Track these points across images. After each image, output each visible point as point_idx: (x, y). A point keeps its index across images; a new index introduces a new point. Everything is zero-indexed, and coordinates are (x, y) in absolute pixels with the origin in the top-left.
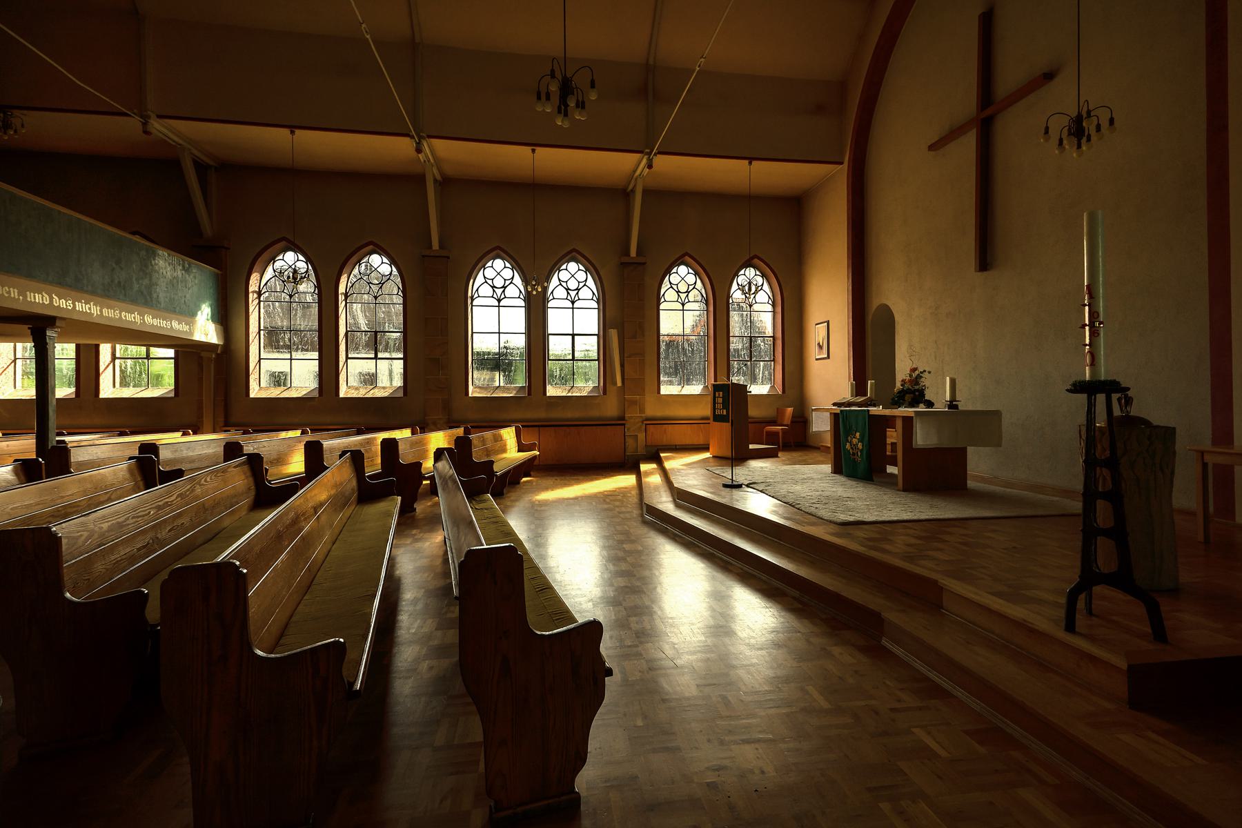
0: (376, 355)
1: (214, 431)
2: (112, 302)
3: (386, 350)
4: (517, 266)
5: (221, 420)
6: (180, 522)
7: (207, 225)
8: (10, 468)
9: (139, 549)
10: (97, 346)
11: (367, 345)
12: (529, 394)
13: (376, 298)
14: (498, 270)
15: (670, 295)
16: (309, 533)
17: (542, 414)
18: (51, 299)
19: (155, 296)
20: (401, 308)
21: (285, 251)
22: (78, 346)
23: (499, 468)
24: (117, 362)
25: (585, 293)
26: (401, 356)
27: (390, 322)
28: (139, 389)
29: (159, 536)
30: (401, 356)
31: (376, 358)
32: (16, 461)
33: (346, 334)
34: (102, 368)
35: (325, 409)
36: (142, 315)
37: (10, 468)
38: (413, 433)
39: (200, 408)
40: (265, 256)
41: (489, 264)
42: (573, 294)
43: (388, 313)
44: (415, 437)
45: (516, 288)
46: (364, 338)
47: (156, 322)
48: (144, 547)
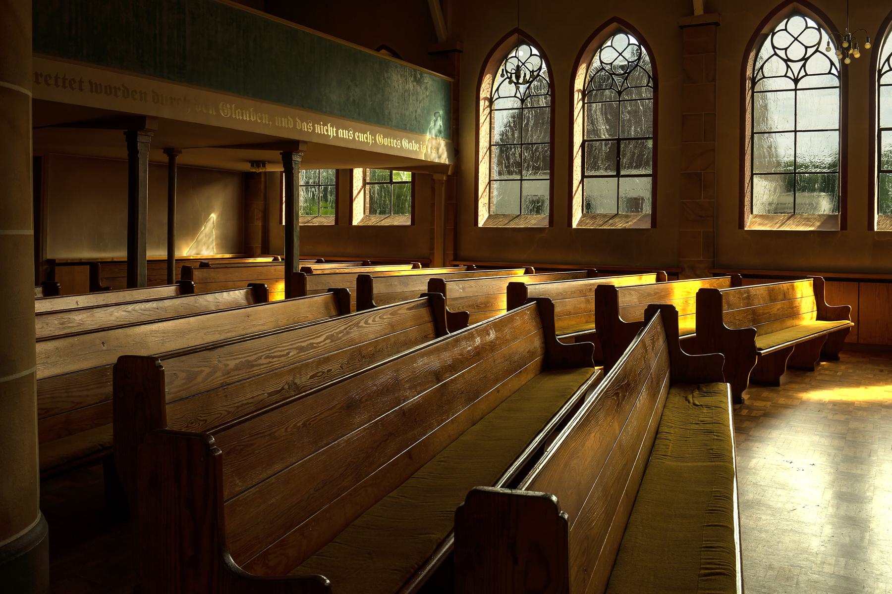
0: (368, 183)
1: (444, 265)
2: (347, 123)
3: (630, 167)
4: (825, 22)
5: (450, 252)
6: (325, 368)
7: (442, 30)
8: (243, 292)
9: (270, 394)
10: (351, 171)
11: (608, 158)
12: (844, 227)
13: (620, 93)
14: (798, 34)
15: (775, 67)
16: (417, 407)
17: (865, 261)
18: (295, 122)
19: (386, 112)
20: (650, 104)
21: (516, 46)
22: (337, 171)
23: (768, 342)
24: (368, 187)
25: (818, 64)
26: (650, 172)
27: (638, 123)
28: (383, 216)
29: (297, 381)
30: (650, 172)
31: (618, 175)
32: (249, 285)
33: (583, 146)
34: (355, 193)
35: (556, 245)
36: (373, 134)
37: (243, 292)
38: (659, 279)
39: (432, 239)
40: (497, 54)
41: (782, 26)
42: (796, 67)
43: (635, 113)
44: (661, 286)
45: (824, 63)
46: (605, 149)
47: (386, 141)
48: (277, 392)
